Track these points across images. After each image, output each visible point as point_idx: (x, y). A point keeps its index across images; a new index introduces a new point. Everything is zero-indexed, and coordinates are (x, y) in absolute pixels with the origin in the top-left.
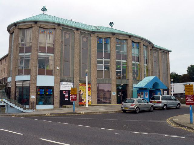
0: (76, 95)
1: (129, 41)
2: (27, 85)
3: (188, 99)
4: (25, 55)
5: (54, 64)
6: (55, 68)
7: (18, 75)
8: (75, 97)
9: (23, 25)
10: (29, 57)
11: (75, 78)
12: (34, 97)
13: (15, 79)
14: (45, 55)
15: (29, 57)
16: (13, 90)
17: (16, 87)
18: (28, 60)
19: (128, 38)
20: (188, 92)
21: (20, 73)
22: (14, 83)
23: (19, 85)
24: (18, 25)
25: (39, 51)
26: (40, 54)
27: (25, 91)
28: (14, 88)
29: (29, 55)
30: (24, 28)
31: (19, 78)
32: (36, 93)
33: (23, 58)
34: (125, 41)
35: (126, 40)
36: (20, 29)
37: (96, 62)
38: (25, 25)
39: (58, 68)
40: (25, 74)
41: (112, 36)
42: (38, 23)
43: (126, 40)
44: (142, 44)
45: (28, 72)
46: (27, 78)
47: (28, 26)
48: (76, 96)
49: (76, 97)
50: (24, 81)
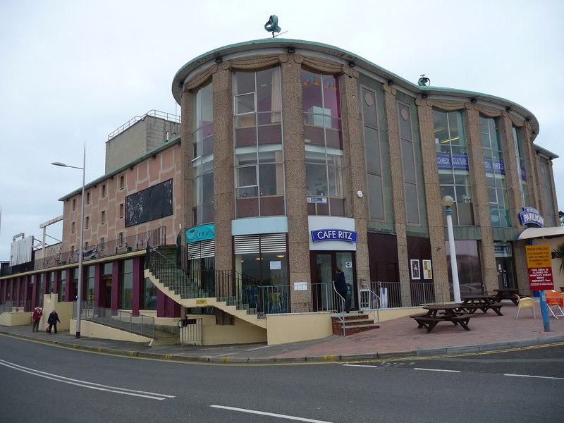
0: (550, 269)
1: (472, 113)
2: (278, 247)
3: (535, 278)
4: (260, 153)
5: (350, 182)
6: (352, 192)
7: (240, 217)
8: (546, 278)
9: (247, 59)
10: (274, 160)
11: (397, 225)
12: (305, 288)
13: (230, 231)
14: (255, 154)
15: (274, 160)
16: (222, 265)
17: (234, 256)
18: (269, 170)
19: (469, 106)
20: (535, 263)
21: (247, 209)
22: (228, 243)
23: (244, 249)
24: (226, 59)
25: (307, 141)
26: (308, 148)
27: (207, 266)
28: (230, 258)
29: (273, 153)
30: (253, 66)
31: (241, 226)
32: (308, 276)
33: (256, 162)
34: (458, 116)
35: (461, 111)
36: (233, 70)
37: (436, 180)
38: (254, 58)
39: (360, 194)
40: (264, 214)
41: (423, 101)
42: (297, 52)
43: (461, 111)
44: (508, 123)
45: (275, 208)
46: (278, 224)
47: (267, 59)
48: (550, 271)
49: (551, 278)
50: (261, 236)
